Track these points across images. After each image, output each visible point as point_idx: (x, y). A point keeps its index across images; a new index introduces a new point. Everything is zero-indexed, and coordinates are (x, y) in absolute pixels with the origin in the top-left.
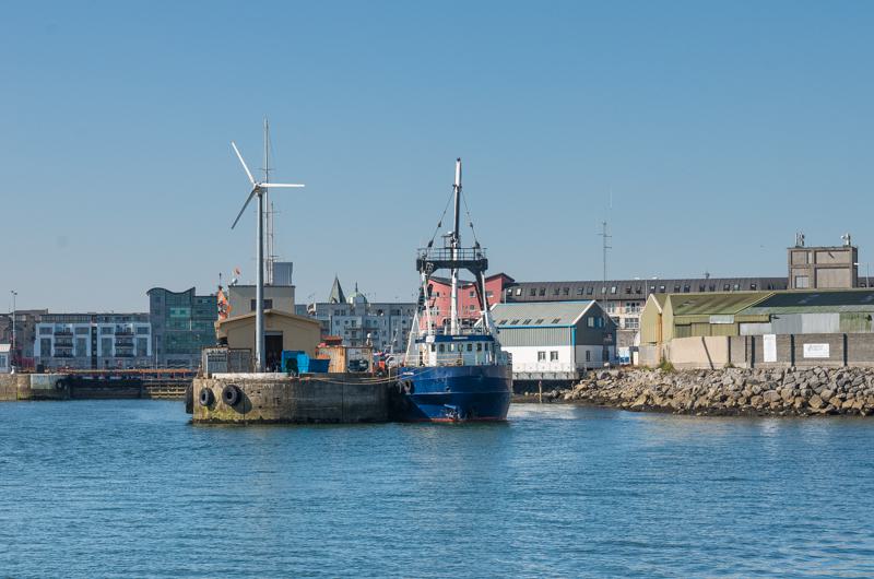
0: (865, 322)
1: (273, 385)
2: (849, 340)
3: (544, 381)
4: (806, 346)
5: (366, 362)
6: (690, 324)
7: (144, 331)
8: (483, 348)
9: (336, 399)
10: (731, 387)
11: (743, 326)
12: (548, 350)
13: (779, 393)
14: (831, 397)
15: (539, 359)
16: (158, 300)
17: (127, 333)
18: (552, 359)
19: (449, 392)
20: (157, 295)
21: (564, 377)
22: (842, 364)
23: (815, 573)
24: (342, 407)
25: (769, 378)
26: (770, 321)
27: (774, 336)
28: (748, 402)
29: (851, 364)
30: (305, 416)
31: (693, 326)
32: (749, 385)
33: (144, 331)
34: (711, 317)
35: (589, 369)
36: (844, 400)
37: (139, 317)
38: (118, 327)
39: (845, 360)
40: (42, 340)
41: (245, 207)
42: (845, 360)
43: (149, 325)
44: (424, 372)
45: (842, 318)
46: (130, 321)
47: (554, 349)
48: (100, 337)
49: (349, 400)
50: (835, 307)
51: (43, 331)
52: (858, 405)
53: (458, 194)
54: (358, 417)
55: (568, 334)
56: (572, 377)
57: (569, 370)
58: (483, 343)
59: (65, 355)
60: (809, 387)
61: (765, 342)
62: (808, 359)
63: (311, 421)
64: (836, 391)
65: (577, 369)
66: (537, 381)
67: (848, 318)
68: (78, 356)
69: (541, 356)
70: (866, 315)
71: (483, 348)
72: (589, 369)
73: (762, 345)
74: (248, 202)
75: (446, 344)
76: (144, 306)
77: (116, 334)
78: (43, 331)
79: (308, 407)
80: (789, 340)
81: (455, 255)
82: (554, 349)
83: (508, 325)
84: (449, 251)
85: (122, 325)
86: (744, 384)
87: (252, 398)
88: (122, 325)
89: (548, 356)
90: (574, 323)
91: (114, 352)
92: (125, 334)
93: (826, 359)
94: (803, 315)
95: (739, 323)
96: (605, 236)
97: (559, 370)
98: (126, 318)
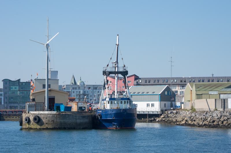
3: (149, 114)
6: (202, 94)
8: (126, 102)
10: (216, 118)
12: (150, 103)
15: (147, 106)
19: (114, 118)
21: (157, 113)
28: (223, 123)
31: (203, 95)
32: (223, 117)
44: (105, 111)
47: (153, 103)
55: (158, 97)
56: (159, 113)
57: (158, 111)
69: (148, 105)
71: (126, 102)
81: (119, 70)
82: (153, 103)
83: (136, 94)
86: (221, 117)
90: (160, 93)
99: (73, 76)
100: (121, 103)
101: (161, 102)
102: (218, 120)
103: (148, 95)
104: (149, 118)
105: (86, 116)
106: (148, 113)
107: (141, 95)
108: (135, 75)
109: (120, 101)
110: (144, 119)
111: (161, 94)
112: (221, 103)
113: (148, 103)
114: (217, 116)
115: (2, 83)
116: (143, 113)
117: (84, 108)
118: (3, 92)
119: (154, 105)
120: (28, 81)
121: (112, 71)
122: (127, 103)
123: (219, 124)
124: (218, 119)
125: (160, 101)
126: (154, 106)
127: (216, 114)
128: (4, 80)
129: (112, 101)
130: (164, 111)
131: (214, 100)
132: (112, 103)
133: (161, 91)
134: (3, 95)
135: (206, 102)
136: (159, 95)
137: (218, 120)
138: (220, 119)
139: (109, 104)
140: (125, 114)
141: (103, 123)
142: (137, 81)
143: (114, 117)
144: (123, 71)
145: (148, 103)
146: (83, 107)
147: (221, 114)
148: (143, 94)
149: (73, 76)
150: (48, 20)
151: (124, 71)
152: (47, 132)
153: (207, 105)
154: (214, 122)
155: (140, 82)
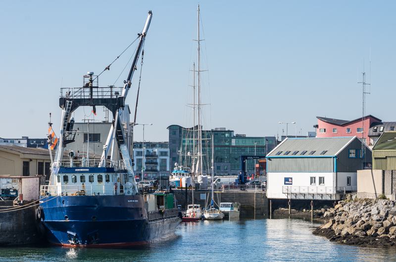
3: (315, 201)
5: (15, 191)
6: (386, 158)
7: (165, 154)
8: (104, 179)
10: (375, 218)
12: (317, 175)
15: (311, 183)
16: (175, 133)
17: (154, 155)
18: (320, 183)
19: (68, 220)
20: (176, 131)
21: (329, 198)
28: (387, 231)
31: (388, 159)
32: (390, 216)
33: (165, 154)
35: (347, 192)
37: (162, 145)
38: (148, 151)
43: (168, 150)
44: (52, 200)
46: (156, 147)
47: (322, 175)
53: (141, 41)
55: (331, 163)
56: (334, 198)
57: (331, 192)
58: (104, 175)
59: (152, 170)
65: (338, 192)
66: (310, 201)
68: (161, 170)
69: (312, 180)
71: (104, 179)
72: (347, 192)
75: (110, 175)
76: (165, 137)
77: (146, 156)
81: (94, 94)
82: (322, 175)
83: (306, 155)
84: (88, 90)
85: (150, 150)
86: (387, 215)
88: (150, 150)
89: (317, 180)
90: (335, 155)
92: (152, 156)
96: (364, 83)
97: (323, 192)
98: (153, 145)
99: (318, 117)
100: (91, 181)
101: (338, 173)
102: (378, 224)
103: (315, 158)
104: (315, 209)
105: (5, 214)
106: (312, 198)
107: (309, 158)
108: (371, 117)
109: (87, 176)
110: (306, 210)
111: (338, 155)
112: (391, 180)
113: (313, 175)
114: (379, 213)
115: (168, 130)
116: (321, 199)
117: (14, 193)
118: (170, 148)
119: (323, 181)
120: (214, 129)
121: (83, 97)
122: (108, 181)
123: (378, 235)
124: (378, 220)
125: (337, 172)
126: (323, 183)
127: (378, 209)
128: (170, 126)
129: (67, 174)
130: (345, 193)
131: (380, 171)
132: (66, 179)
133: (343, 146)
134: (169, 154)
135: (338, 177)
136: (335, 159)
137: (378, 224)
138: (384, 222)
139: (60, 183)
140: (95, 208)
141: (52, 232)
142: (375, 128)
143: (66, 217)
144: (110, 97)
145: (313, 175)
146: (11, 190)
147: (388, 208)
148: (279, 156)
149: (318, 117)
150: (199, 10)
151: (115, 97)
152: (297, 223)
153: (338, 182)
154: (368, 227)
155: (381, 130)
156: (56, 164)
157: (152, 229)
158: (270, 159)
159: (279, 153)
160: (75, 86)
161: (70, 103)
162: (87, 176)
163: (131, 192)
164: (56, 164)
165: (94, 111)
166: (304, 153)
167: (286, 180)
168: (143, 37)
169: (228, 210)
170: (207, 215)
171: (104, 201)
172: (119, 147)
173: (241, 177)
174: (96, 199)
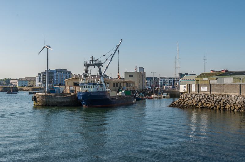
0: (239, 80)
1: (41, 96)
2: (212, 85)
4: (201, 87)
5: (74, 90)
8: (92, 87)
9: (56, 100)
10: (182, 99)
11: (211, 81)
13: (193, 101)
14: (204, 103)
19: (81, 99)
22: (209, 93)
23: (202, 155)
24: (58, 102)
25: (192, 96)
26: (216, 80)
27: (194, 84)
28: (184, 103)
29: (212, 93)
30: (48, 104)
34: (203, 79)
36: (207, 104)
39: (211, 92)
40: (161, 82)
41: (41, 51)
42: (211, 92)
45: (233, 79)
48: (170, 82)
49: (60, 100)
50: (231, 76)
51: (161, 80)
52: (210, 106)
54: (63, 105)
60: (200, 99)
61: (192, 86)
62: (202, 91)
63: (49, 105)
64: (206, 101)
67: (235, 79)
70: (239, 78)
71: (92, 87)
73: (192, 87)
74: (41, 51)
75: (95, 86)
78: (161, 80)
79: (49, 102)
80: (239, 86)
86: (186, 98)
87: (38, 99)
91: (162, 84)
93: (206, 91)
94: (224, 78)
95: (209, 80)
149: (211, 70)
156: (153, 79)
157: (46, 102)
158: (180, 81)
159: (183, 80)
160: (88, 59)
161: (87, 65)
162: (88, 86)
163: (102, 90)
164: (153, 79)
165: (95, 67)
166: (189, 80)
167: (184, 87)
168: (118, 46)
169: (165, 95)
170: (157, 97)
171: (92, 93)
172: (188, 75)
173: (173, 86)
174: (90, 93)
